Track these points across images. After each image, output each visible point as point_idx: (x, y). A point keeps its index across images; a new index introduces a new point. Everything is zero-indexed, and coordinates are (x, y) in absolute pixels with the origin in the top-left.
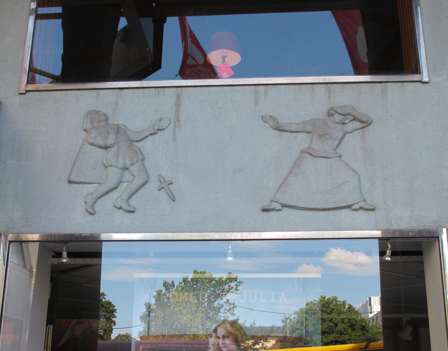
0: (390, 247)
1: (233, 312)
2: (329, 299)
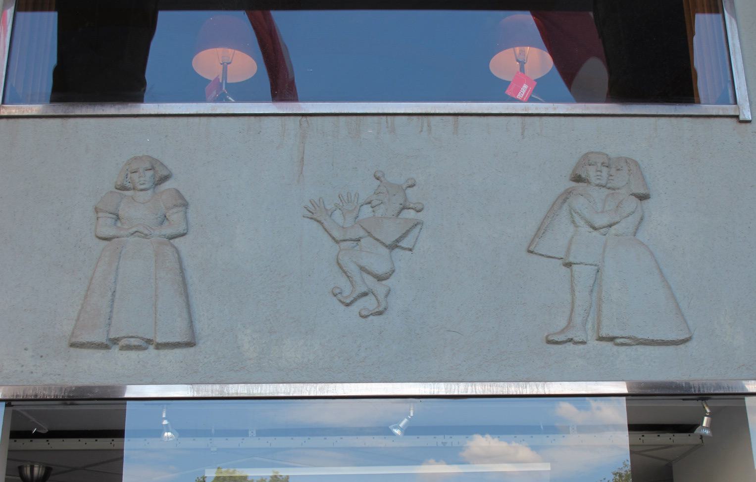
0: (708, 411)
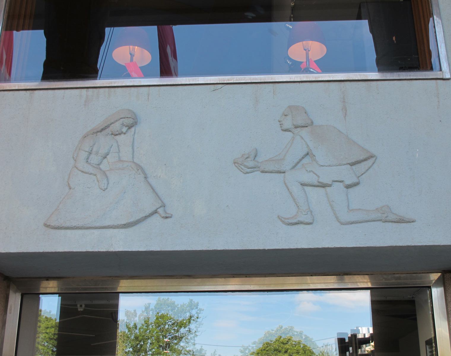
1: (194, 341)
2: (286, 329)
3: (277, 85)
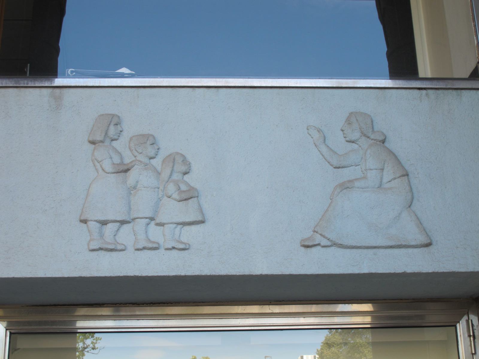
3: (387, 91)
